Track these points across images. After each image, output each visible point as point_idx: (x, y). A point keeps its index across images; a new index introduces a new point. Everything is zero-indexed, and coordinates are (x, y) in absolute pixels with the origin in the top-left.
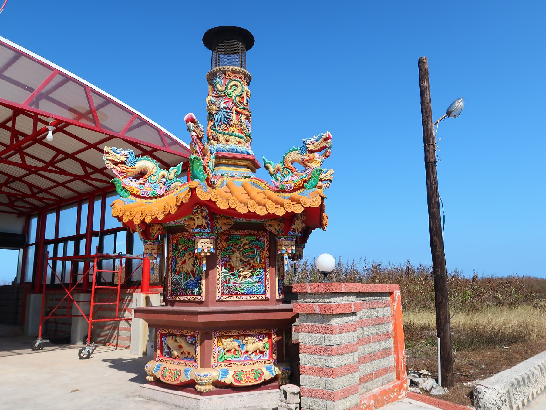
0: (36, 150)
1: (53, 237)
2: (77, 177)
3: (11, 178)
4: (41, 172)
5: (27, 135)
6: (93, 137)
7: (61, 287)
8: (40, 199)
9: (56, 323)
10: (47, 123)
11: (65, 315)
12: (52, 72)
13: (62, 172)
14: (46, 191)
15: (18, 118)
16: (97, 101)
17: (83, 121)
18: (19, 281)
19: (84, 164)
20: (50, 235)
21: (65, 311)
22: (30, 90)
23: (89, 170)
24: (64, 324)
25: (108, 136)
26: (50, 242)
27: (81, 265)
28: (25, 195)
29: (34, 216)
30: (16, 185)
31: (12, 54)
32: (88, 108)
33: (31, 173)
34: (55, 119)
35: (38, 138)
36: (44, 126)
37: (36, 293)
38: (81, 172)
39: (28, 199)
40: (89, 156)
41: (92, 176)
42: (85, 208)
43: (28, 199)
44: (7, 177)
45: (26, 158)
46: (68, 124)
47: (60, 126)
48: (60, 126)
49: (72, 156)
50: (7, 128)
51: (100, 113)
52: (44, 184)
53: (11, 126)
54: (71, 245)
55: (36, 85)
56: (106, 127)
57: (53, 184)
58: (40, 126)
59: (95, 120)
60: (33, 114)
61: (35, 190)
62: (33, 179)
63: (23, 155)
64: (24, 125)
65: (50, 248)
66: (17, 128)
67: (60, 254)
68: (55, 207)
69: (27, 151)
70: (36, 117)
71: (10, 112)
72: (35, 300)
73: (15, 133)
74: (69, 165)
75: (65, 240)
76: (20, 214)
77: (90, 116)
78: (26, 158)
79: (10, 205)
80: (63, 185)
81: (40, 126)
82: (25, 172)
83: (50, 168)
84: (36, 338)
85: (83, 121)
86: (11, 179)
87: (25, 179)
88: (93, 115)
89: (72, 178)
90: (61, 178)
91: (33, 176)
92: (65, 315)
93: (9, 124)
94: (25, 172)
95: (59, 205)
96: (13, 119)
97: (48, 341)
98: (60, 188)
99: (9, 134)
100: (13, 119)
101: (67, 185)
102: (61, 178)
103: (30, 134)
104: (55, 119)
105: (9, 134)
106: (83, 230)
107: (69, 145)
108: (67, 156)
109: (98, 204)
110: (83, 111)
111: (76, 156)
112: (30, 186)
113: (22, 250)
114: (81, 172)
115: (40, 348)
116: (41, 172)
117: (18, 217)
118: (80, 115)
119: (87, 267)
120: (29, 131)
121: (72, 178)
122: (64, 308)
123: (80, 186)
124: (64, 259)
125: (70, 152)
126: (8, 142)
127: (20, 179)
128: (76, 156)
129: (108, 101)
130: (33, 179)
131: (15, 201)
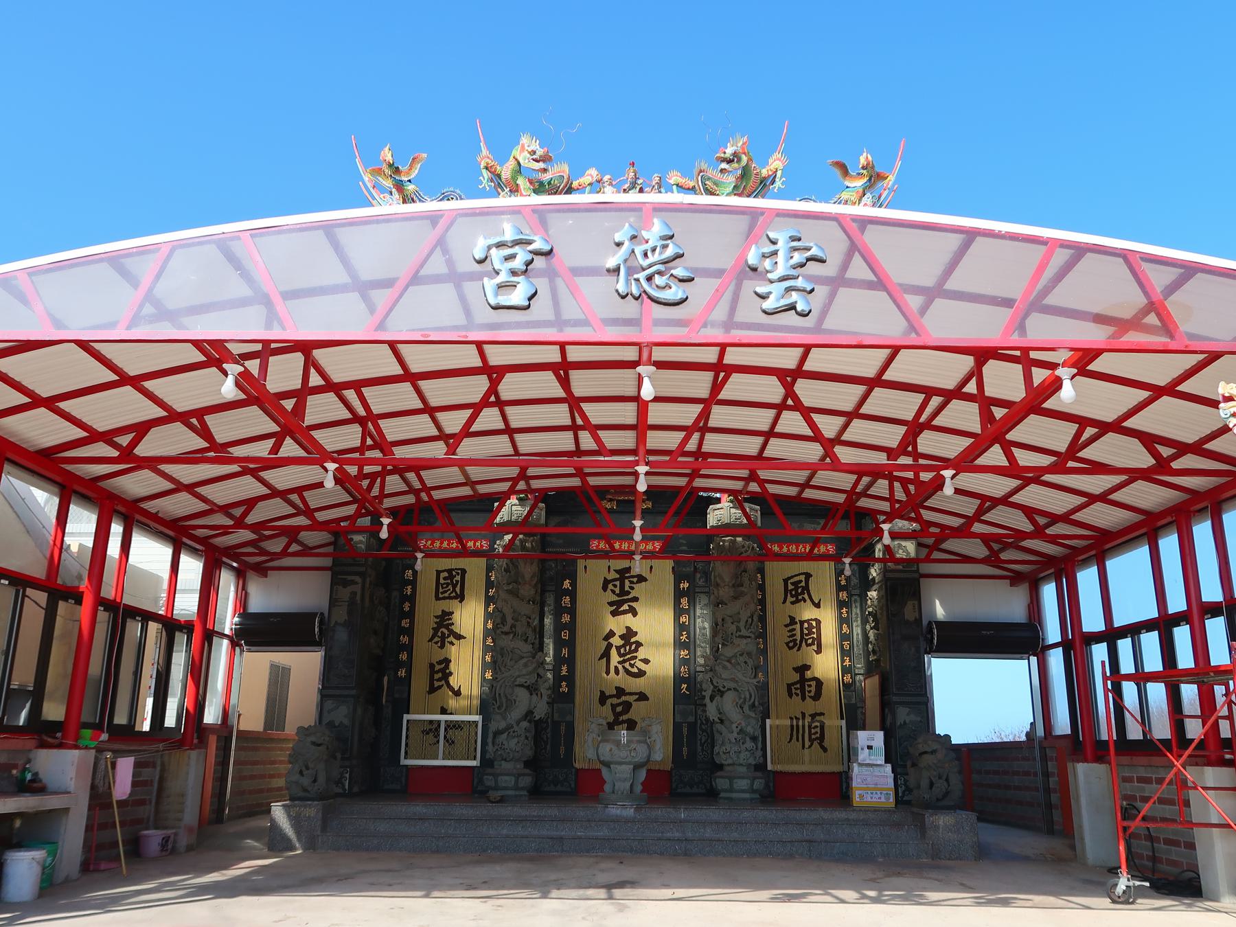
0: (1031, 430)
1: (1100, 626)
2: (1135, 475)
3: (987, 502)
4: (1048, 478)
5: (1014, 403)
6: (1161, 370)
7: (1147, 747)
8: (1053, 539)
9: (1150, 838)
10: (1052, 366)
11: (1174, 821)
12: (1043, 248)
13: (1098, 468)
14: (1066, 518)
15: (985, 369)
16: (1159, 278)
17: (1133, 337)
18: (1040, 732)
19: (1149, 440)
20: (1092, 621)
21: (1168, 811)
22: (1007, 303)
23: (1166, 452)
24: (1175, 843)
25: (1201, 357)
26: (1096, 638)
27: (1189, 692)
28: (1020, 535)
29: (1046, 579)
30: (1000, 515)
31: (955, 240)
32: (1142, 301)
33: (1027, 482)
34: (1072, 349)
35: (1037, 401)
36: (1047, 372)
37: (1086, 761)
38: (1146, 461)
39: (1028, 543)
40: (1168, 418)
41: (1175, 465)
42: (1169, 545)
43: (1028, 543)
44: (978, 502)
45: (1017, 452)
46: (1095, 353)
47: (1083, 361)
48: (1083, 361)
49: (1116, 426)
50: (969, 398)
51: (1174, 304)
52: (1058, 503)
53: (975, 392)
54: (1150, 641)
55: (1015, 290)
56: (1192, 336)
57: (1080, 500)
58: (1039, 375)
59: (1168, 326)
60: (1018, 353)
61: (1042, 521)
62: (1033, 496)
63: (1007, 447)
64: (1004, 382)
65: (1100, 652)
66: (989, 391)
67: (1127, 666)
68: (1093, 552)
69: (1009, 437)
70: (1024, 358)
71: (968, 362)
72: (1088, 778)
73: (986, 403)
74: (1109, 449)
75: (1133, 630)
76: (1016, 579)
77: (1152, 319)
78: (1017, 452)
79: (992, 560)
80: (1103, 498)
81: (1039, 375)
82: (1015, 483)
83: (1071, 464)
84: (1114, 871)
85: (1133, 337)
86: (988, 504)
87: (1016, 499)
88: (1158, 315)
89: (1124, 477)
90: (1096, 484)
91: (1033, 488)
92: (1174, 821)
93: (971, 388)
94: (1015, 483)
95: (1102, 546)
96: (976, 373)
97: (1147, 884)
98: (1098, 506)
99: (974, 408)
100: (976, 373)
101: (1113, 497)
102: (1096, 484)
103: (1018, 400)
104: (1072, 349)
105: (974, 408)
106: (1177, 602)
107: (1107, 402)
108: (1105, 428)
109: (1202, 531)
110: (1127, 314)
111: (1125, 424)
112: (1029, 512)
113: (1034, 660)
114: (1146, 461)
115: (1127, 899)
116: (1048, 478)
117: (1012, 585)
118: (1122, 325)
119: (1207, 699)
120: (1016, 392)
121: (1124, 477)
122: (1170, 802)
123: (1148, 496)
124: (1141, 678)
125: (1109, 417)
126: (976, 428)
127: (1005, 501)
128: (1125, 424)
129: (1190, 270)
130: (1033, 496)
131: (1002, 550)
